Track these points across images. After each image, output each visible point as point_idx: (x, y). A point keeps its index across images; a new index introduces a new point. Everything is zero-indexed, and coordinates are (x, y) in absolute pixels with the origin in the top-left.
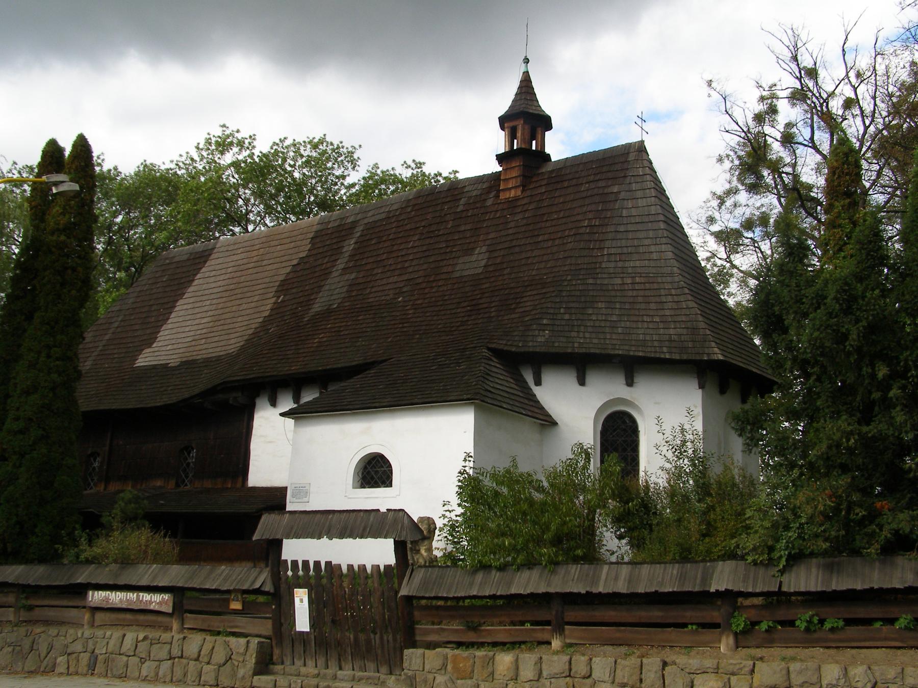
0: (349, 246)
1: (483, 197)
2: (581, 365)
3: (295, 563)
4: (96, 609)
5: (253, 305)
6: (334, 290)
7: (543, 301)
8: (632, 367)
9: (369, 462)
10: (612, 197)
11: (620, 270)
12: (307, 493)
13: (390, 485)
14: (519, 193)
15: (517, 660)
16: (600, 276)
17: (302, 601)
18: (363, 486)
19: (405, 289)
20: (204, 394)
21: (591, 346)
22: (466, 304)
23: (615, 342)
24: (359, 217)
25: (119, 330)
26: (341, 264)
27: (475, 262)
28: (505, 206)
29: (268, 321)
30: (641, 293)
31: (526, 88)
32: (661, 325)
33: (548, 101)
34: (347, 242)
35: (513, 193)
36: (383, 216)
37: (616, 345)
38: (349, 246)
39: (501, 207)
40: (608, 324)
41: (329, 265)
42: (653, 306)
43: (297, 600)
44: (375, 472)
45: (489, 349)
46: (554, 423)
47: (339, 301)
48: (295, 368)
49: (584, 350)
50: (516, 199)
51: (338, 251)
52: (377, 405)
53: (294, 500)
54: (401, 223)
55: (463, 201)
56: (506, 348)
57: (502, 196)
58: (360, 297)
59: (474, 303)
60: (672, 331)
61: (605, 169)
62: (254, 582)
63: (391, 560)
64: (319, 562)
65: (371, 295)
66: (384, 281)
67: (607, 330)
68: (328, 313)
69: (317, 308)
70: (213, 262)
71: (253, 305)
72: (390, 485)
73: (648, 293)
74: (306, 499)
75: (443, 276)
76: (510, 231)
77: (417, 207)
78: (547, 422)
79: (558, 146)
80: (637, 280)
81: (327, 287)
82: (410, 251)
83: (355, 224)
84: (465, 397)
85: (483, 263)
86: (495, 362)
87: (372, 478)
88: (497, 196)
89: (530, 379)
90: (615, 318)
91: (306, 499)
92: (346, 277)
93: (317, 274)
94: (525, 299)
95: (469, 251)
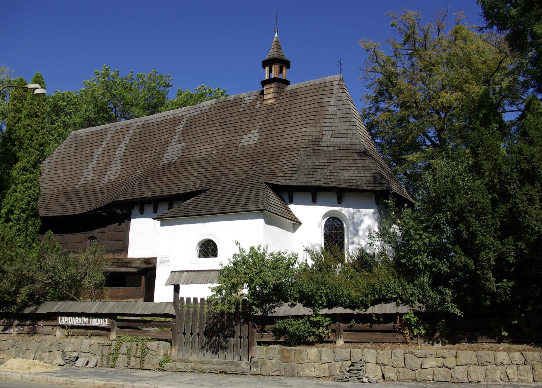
0: (180, 128)
1: (254, 103)
3: (188, 299)
4: (63, 327)
7: (292, 158)
8: (341, 194)
9: (204, 244)
10: (326, 104)
11: (331, 143)
13: (216, 256)
15: (320, 353)
16: (322, 145)
19: (213, 152)
20: (103, 208)
21: (321, 182)
22: (249, 160)
23: (333, 180)
24: (185, 113)
25: (49, 173)
26: (176, 138)
27: (251, 138)
30: (344, 155)
32: (356, 172)
34: (178, 127)
35: (270, 101)
36: (198, 113)
37: (332, 181)
38: (180, 128)
39: (264, 108)
40: (328, 171)
41: (169, 139)
42: (351, 162)
44: (208, 249)
45: (266, 183)
47: (176, 158)
48: (312, 180)
49: (317, 185)
50: (272, 105)
51: (174, 132)
52: (209, 213)
53: (161, 265)
54: (209, 117)
55: (243, 106)
56: (275, 183)
58: (189, 156)
59: (254, 159)
60: (362, 175)
61: (321, 89)
65: (195, 155)
66: (202, 148)
67: (328, 174)
68: (170, 165)
69: (164, 162)
72: (216, 256)
73: (348, 155)
74: (167, 264)
75: (235, 145)
76: (271, 122)
77: (216, 109)
80: (342, 148)
81: (169, 151)
82: (215, 132)
84: (214, 211)
85: (257, 138)
86: (270, 191)
87: (206, 252)
88: (261, 103)
90: (331, 168)
91: (167, 264)
92: (180, 145)
93: (162, 144)
94: (282, 157)
95: (249, 132)
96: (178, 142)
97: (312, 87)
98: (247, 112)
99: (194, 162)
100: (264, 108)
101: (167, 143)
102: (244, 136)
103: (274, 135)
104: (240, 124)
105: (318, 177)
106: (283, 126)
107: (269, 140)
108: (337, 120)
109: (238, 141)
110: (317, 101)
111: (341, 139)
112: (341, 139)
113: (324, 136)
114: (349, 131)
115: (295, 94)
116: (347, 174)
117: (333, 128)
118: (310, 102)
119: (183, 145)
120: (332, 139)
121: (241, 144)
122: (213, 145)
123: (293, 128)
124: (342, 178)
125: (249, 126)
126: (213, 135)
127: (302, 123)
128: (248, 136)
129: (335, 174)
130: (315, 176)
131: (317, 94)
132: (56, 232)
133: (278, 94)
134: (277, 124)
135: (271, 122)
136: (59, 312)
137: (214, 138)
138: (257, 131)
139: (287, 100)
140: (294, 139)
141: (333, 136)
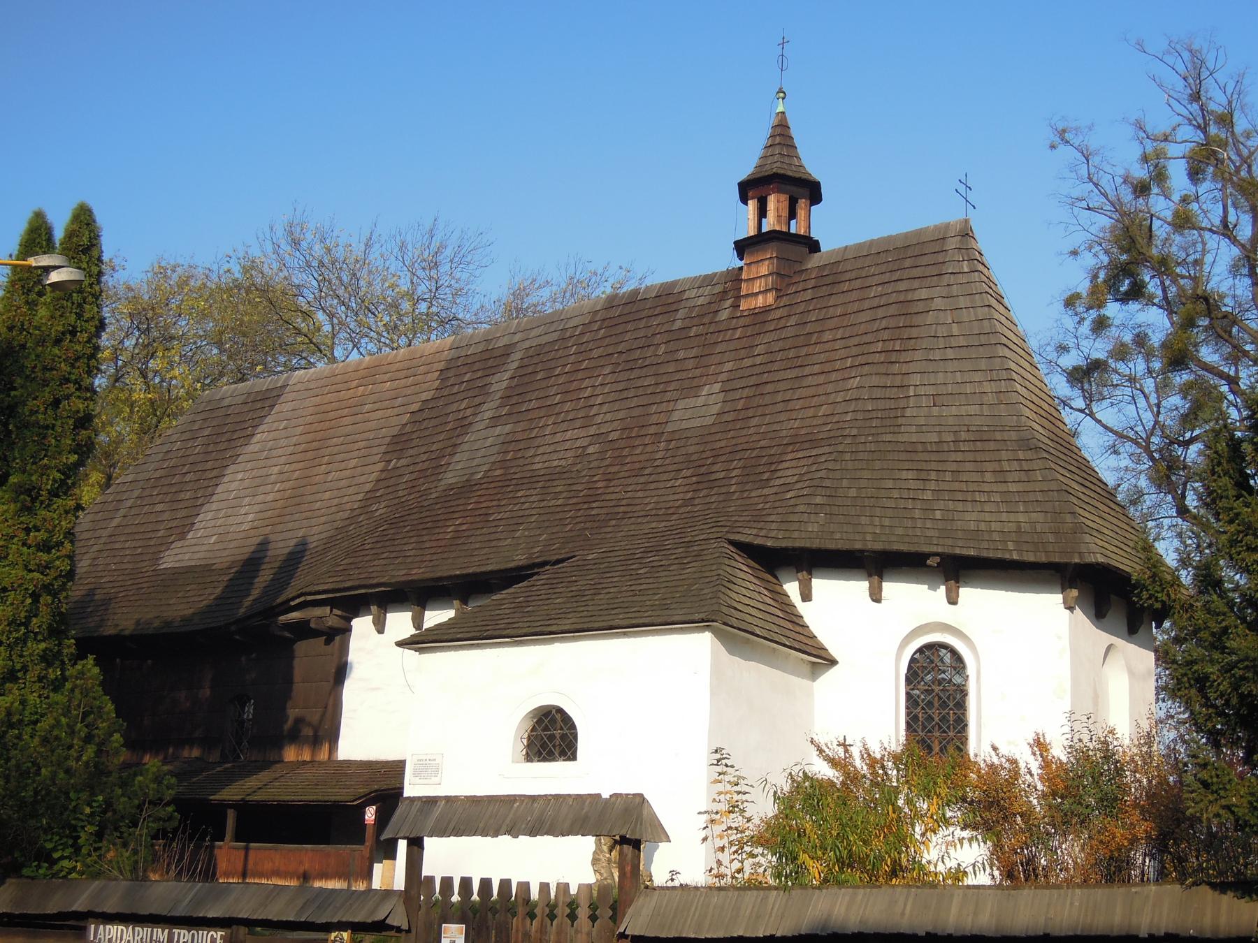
0: (500, 382)
2: (878, 564)
6: (478, 450)
12: (437, 771)
13: (573, 757)
14: (770, 298)
18: (529, 758)
19: (591, 450)
29: (370, 498)
31: (781, 135)
33: (813, 163)
35: (760, 301)
38: (500, 382)
44: (551, 735)
46: (833, 662)
50: (766, 310)
57: (744, 305)
68: (467, 487)
72: (573, 757)
74: (435, 780)
78: (820, 660)
79: (834, 227)
89: (792, 589)
92: (498, 430)
96: (495, 421)
101: (464, 426)
104: (671, 368)
109: (662, 418)
117: (940, 378)
119: (508, 428)
121: (670, 428)
123: (822, 379)
127: (849, 362)
129: (938, 515)
131: (896, 276)
133: (784, 279)
138: (717, 387)
139: (808, 295)
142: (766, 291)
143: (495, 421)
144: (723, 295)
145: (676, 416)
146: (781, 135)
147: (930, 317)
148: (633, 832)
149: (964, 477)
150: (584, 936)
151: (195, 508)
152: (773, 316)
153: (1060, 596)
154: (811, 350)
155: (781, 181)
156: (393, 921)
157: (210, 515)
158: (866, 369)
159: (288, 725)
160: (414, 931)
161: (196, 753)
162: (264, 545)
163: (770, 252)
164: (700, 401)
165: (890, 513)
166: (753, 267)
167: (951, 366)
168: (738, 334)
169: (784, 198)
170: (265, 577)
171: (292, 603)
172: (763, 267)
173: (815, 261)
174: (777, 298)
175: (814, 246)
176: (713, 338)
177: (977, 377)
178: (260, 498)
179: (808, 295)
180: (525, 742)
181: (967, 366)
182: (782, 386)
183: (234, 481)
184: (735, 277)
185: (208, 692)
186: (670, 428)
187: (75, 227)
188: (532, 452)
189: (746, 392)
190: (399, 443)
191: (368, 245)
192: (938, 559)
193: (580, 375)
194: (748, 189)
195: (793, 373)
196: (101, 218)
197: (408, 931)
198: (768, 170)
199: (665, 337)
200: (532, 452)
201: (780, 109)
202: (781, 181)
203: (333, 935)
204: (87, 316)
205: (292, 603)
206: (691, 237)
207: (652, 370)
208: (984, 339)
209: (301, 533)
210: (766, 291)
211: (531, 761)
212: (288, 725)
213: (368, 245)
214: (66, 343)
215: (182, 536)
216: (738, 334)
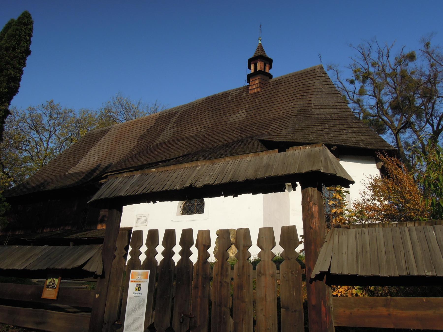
0: (174, 119)
5: (126, 146)
6: (167, 134)
12: (146, 220)
13: (203, 212)
14: (259, 89)
17: (138, 287)
18: (183, 214)
19: (203, 130)
28: (252, 95)
29: (133, 150)
31: (260, 48)
35: (256, 90)
38: (174, 119)
43: (132, 287)
50: (257, 92)
57: (250, 92)
62: (152, 320)
63: (259, 250)
64: (271, 230)
67: (324, 135)
68: (162, 143)
69: (157, 142)
70: (110, 133)
71: (126, 146)
72: (203, 212)
74: (145, 224)
83: (176, 113)
92: (173, 130)
96: (172, 128)
97: (295, 76)
98: (234, 100)
99: (184, 138)
100: (250, 96)
101: (162, 130)
102: (232, 116)
103: (262, 112)
104: (228, 109)
105: (314, 136)
106: (270, 105)
107: (256, 115)
108: (323, 96)
109: (226, 120)
110: (301, 84)
111: (331, 110)
112: (331, 110)
113: (313, 107)
114: (337, 104)
115: (279, 82)
116: (345, 136)
117: (321, 102)
118: (295, 86)
119: (176, 129)
120: (322, 110)
121: (229, 122)
122: (203, 126)
123: (280, 104)
124: (341, 138)
125: (237, 109)
126: (203, 119)
127: (289, 100)
128: (236, 115)
129: (332, 135)
130: (311, 136)
131: (300, 79)
132: (6, 119)
133: (263, 85)
134: (263, 104)
135: (257, 103)
136: (48, 269)
137: (203, 121)
138: (244, 111)
139: (272, 87)
140: (282, 112)
141: (322, 107)
142: (257, 88)
143: (172, 128)
144: (243, 91)
145: (231, 119)
146: (260, 48)
147: (315, 87)
148: (326, 167)
149: (336, 126)
150: (269, 278)
151: (80, 158)
152: (260, 93)
153: (376, 165)
154: (274, 99)
155: (261, 59)
156: (92, 268)
157: (84, 160)
158: (295, 100)
159: (100, 218)
160: (107, 277)
161: (70, 228)
162: (99, 165)
163: (259, 77)
164: (238, 115)
165: (315, 134)
166: (253, 82)
167: (324, 99)
168: (249, 99)
169: (263, 63)
170: (98, 172)
171: (103, 176)
172: (256, 81)
173: (272, 80)
174: (261, 89)
175: (270, 76)
176: (241, 101)
177: (333, 101)
178: (99, 154)
179: (272, 87)
180: (182, 208)
181: (329, 99)
182: (265, 108)
183: (93, 151)
184: (247, 88)
185: (75, 208)
186: (229, 122)
187: (22, 16)
188: (183, 133)
189: (254, 111)
190: (142, 137)
191: (139, 104)
192: (336, 147)
193: (199, 114)
194: (250, 61)
195: (270, 105)
196: (34, 18)
197: (103, 276)
198: (257, 55)
199: (225, 103)
200: (183, 133)
201: (260, 42)
202: (261, 59)
203: (49, 281)
204: (21, 45)
205: (103, 176)
206: (233, 78)
207: (222, 110)
208: (333, 92)
209: (110, 161)
210: (257, 88)
211: (185, 215)
212: (100, 218)
213: (139, 104)
214: (11, 51)
215: (75, 165)
216: (249, 99)
